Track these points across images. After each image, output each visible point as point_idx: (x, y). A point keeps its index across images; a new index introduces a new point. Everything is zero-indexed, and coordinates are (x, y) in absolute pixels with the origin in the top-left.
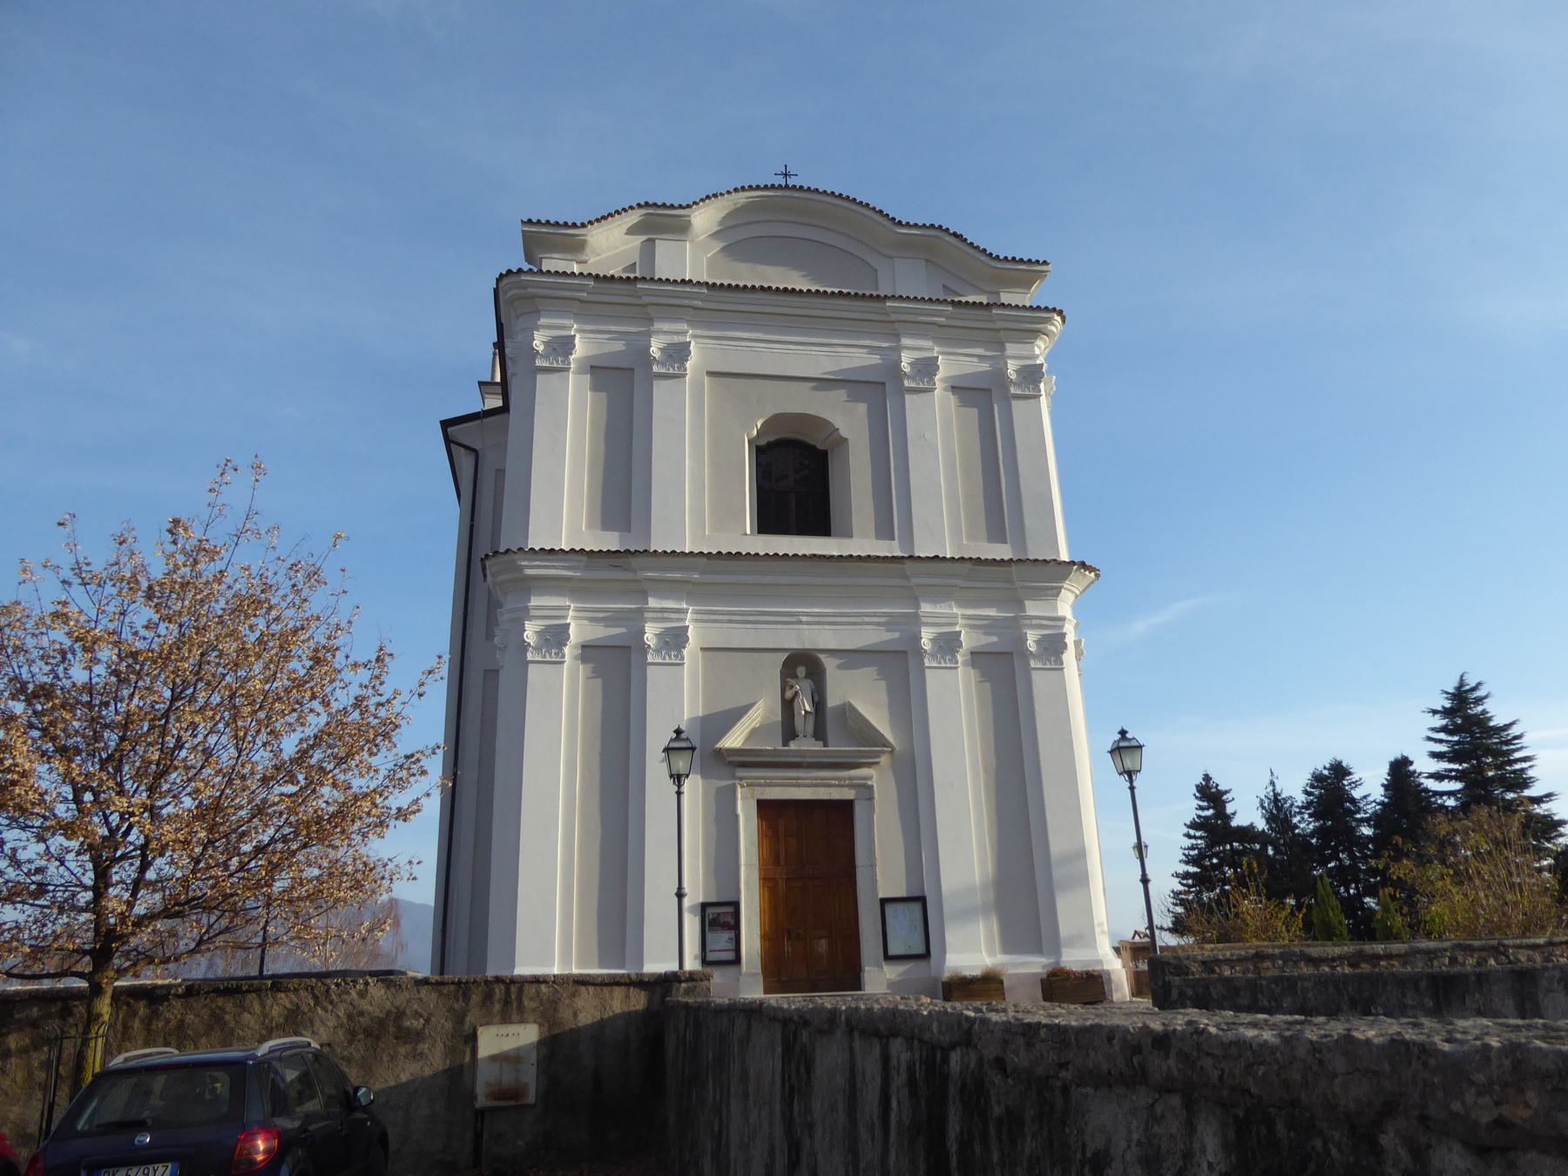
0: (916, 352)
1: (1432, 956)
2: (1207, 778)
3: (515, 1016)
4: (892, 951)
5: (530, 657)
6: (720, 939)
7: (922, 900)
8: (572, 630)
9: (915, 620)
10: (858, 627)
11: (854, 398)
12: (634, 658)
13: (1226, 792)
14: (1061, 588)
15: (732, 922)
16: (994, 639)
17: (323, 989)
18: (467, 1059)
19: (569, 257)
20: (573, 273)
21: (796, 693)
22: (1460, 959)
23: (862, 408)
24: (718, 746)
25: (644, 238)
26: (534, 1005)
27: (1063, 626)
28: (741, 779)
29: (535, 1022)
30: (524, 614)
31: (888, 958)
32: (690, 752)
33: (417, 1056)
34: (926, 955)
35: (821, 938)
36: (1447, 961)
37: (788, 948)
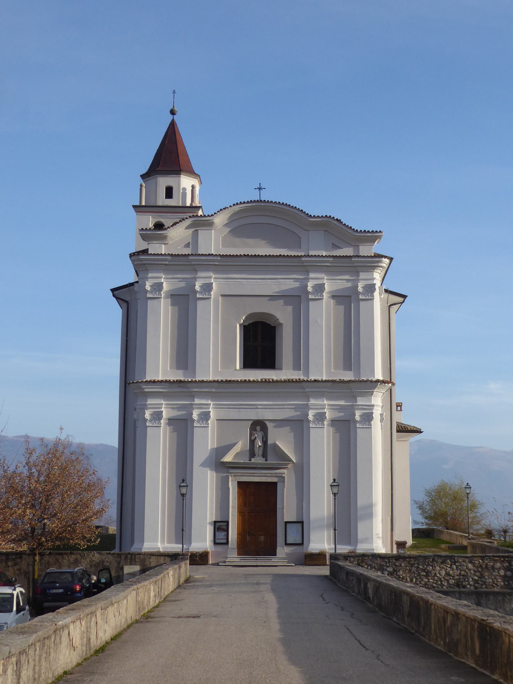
0: (317, 280)
1: (425, 558)
3: (134, 563)
4: (288, 542)
5: (148, 424)
6: (221, 535)
7: (302, 523)
8: (164, 414)
9: (307, 407)
10: (282, 410)
11: (286, 304)
12: (189, 423)
14: (373, 392)
15: (226, 528)
16: (342, 414)
17: (83, 554)
18: (121, 573)
19: (160, 242)
20: (161, 254)
21: (256, 438)
22: (436, 560)
23: (290, 308)
24: (221, 461)
25: (193, 230)
26: (139, 560)
27: (372, 409)
28: (231, 473)
29: (139, 565)
30: (145, 407)
31: (286, 544)
34: (302, 544)
35: (261, 535)
36: (431, 560)
37: (248, 538)
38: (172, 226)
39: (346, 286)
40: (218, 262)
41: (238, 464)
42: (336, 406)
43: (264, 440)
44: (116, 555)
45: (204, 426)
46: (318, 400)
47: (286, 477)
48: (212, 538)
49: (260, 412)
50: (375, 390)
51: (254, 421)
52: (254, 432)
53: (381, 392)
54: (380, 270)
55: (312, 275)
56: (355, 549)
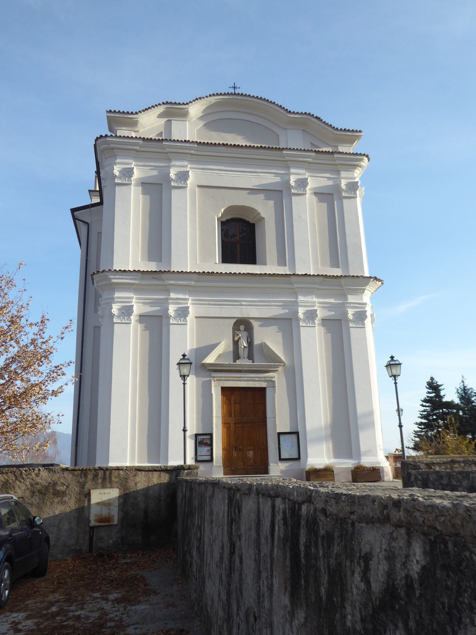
2: (432, 379)
3: (108, 485)
4: (282, 457)
5: (115, 320)
6: (204, 451)
7: (297, 433)
8: (135, 308)
11: (267, 198)
13: (441, 385)
14: (365, 289)
15: (209, 442)
16: (333, 313)
17: (19, 473)
19: (130, 129)
21: (240, 338)
23: (271, 203)
25: (166, 119)
26: (117, 480)
27: (365, 308)
28: (214, 377)
29: (117, 488)
30: (112, 300)
31: (281, 459)
32: (190, 364)
33: (63, 503)
34: (298, 459)
38: (143, 111)
39: (328, 184)
40: (194, 151)
41: (222, 367)
42: (327, 304)
43: (249, 341)
44: (79, 472)
45: (182, 323)
46: (307, 297)
47: (276, 382)
48: (193, 455)
49: (245, 310)
50: (367, 288)
51: (237, 319)
52: (238, 332)
53: (370, 291)
54: (360, 170)
55: (292, 170)
56: (359, 463)
